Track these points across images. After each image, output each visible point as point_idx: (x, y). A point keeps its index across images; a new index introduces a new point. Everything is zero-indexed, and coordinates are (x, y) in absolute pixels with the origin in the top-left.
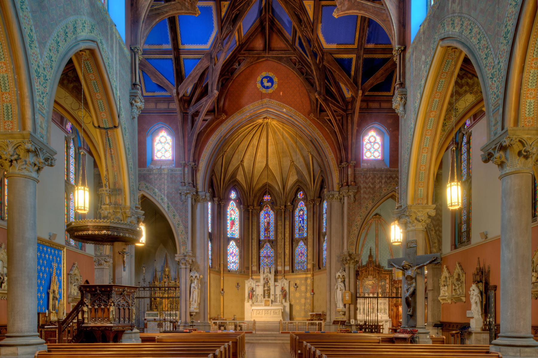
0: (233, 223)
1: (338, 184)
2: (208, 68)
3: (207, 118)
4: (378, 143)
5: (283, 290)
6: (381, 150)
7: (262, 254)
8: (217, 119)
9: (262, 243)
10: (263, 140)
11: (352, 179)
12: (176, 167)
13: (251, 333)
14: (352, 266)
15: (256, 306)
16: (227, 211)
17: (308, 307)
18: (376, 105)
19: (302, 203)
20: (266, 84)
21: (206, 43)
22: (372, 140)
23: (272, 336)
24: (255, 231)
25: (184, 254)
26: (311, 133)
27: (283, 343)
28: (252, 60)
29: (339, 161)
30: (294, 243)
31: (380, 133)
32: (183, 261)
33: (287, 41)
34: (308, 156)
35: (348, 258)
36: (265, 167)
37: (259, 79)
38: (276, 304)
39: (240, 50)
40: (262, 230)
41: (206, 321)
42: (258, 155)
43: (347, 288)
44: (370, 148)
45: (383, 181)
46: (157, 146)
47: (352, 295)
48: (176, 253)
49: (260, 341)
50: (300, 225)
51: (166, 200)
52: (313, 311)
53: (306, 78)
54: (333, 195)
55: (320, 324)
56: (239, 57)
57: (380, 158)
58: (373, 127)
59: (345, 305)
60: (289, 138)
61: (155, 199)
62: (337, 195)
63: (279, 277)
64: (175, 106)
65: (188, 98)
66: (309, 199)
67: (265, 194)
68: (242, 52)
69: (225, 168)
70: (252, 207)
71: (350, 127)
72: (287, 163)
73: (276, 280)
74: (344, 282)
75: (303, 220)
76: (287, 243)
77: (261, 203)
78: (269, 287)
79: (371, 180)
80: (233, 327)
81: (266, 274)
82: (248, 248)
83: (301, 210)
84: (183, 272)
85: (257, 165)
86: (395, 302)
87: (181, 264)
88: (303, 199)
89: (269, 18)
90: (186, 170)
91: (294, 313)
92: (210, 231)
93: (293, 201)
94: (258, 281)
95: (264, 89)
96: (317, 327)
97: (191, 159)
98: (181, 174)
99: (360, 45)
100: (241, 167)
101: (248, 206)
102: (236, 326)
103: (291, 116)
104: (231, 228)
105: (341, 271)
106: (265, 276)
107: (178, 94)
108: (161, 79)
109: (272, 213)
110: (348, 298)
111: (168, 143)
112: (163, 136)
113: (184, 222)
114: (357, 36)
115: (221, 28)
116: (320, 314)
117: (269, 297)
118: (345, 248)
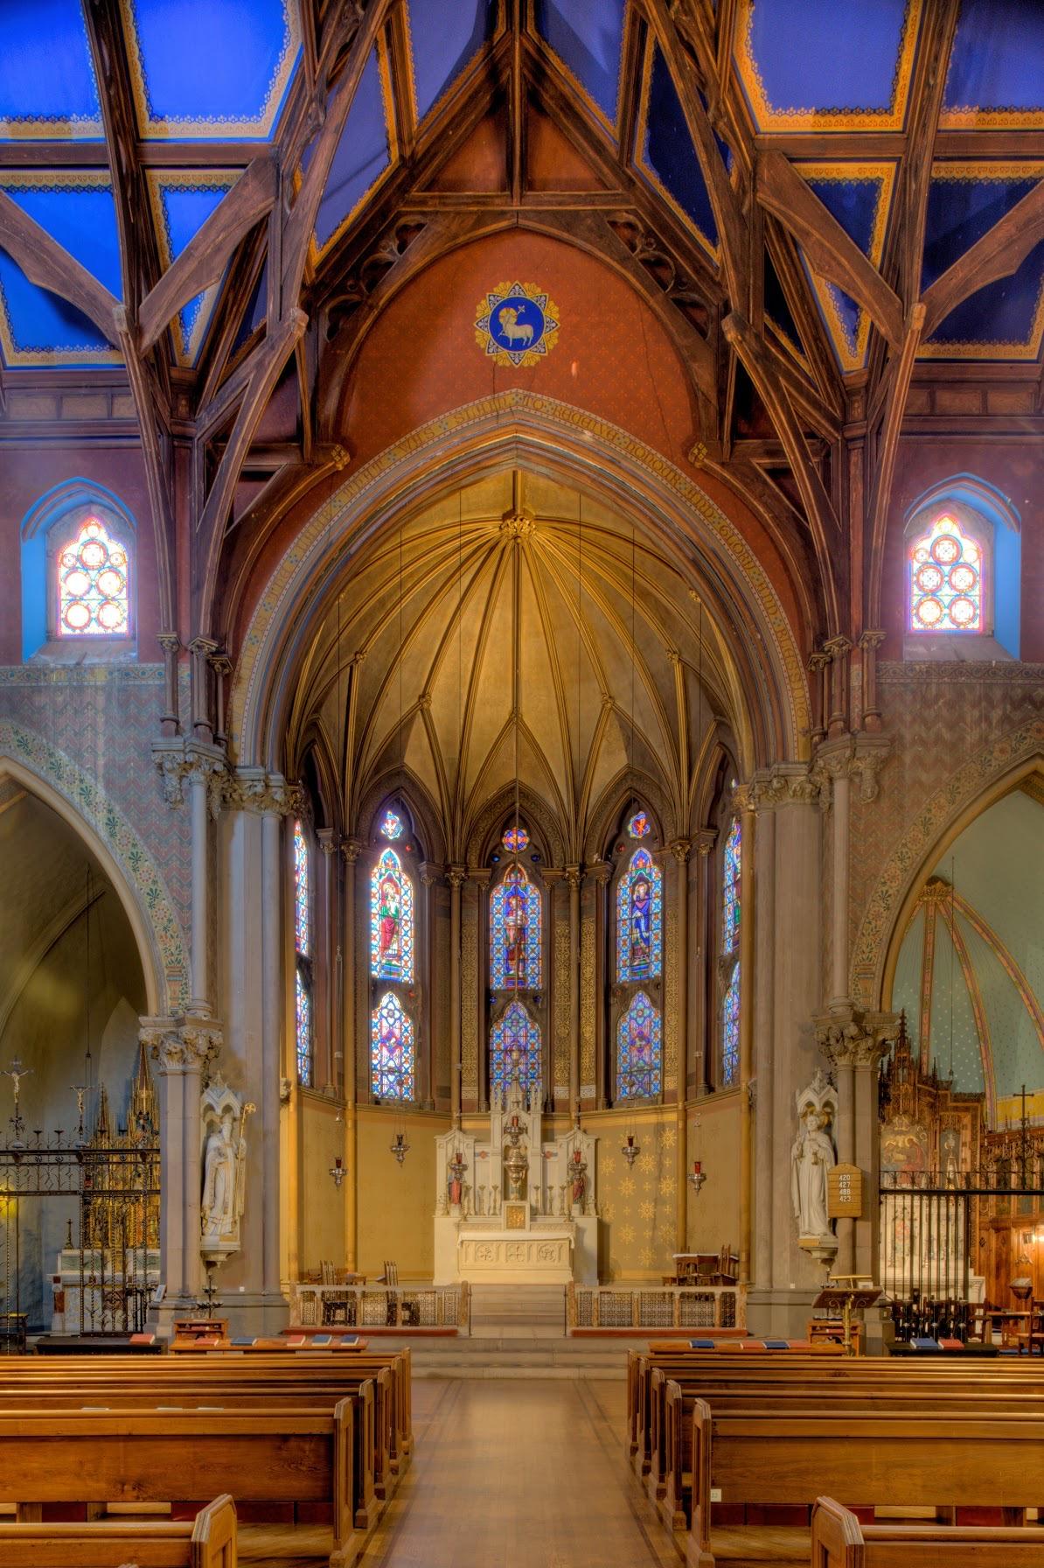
0: (391, 927)
1: (806, 732)
2: (260, 228)
3: (266, 463)
4: (967, 566)
5: (577, 1166)
6: (983, 596)
7: (496, 1043)
8: (311, 466)
9: (498, 1003)
10: (502, 615)
11: (870, 706)
12: (143, 658)
13: (452, 1334)
14: (864, 1063)
15: (476, 1227)
16: (369, 886)
17: (668, 1232)
18: (967, 401)
19: (642, 856)
20: (513, 331)
21: (252, 109)
22: (946, 552)
23: (537, 1347)
24: (472, 958)
25: (174, 1014)
26: (694, 530)
27: (584, 1380)
28: (454, 228)
29: (810, 636)
30: (613, 1000)
31: (981, 525)
32: (171, 1045)
33: (599, 147)
34: (670, 669)
35: (852, 1030)
36: (510, 720)
37: (484, 309)
38: (550, 1220)
39: (404, 189)
40: (498, 954)
41: (271, 1288)
42: (482, 678)
43: (844, 1155)
44: (939, 588)
45: (996, 715)
46: (71, 584)
47: (864, 1180)
48: (145, 1013)
49: (488, 1372)
50: (637, 934)
51: (101, 793)
52: (685, 1249)
53: (676, 301)
54: (785, 778)
55: (729, 1300)
56: (400, 215)
57: (976, 625)
58: (949, 500)
59: (833, 1223)
60: (600, 602)
61: (59, 793)
62: (799, 779)
63: (558, 1125)
64: (132, 407)
65: (190, 377)
66: (669, 835)
67: (507, 826)
68: (415, 193)
69: (358, 719)
70: (459, 870)
71: (856, 496)
72: (589, 704)
73: (547, 1136)
74: (827, 1128)
75: (647, 916)
76: (589, 1002)
77: (492, 856)
78: (523, 1158)
79: (945, 712)
80: (381, 1308)
81: (513, 1101)
82: (449, 1029)
83: (641, 879)
84: (173, 1087)
85: (480, 716)
86: (992, 1214)
87: (165, 1059)
88: (648, 841)
89: (525, 52)
90: (185, 671)
91: (613, 1254)
92: (304, 952)
93: (609, 850)
94: (482, 1137)
95: (504, 352)
96: (717, 1308)
97: (204, 625)
98: (163, 687)
99: (919, 113)
100: (419, 720)
101: (447, 868)
102: (392, 1308)
103: (612, 461)
104: (386, 945)
105: (816, 1084)
106: (507, 1119)
107: (137, 331)
108: (65, 269)
109: (532, 893)
110: (848, 1194)
111: (113, 569)
112: (92, 541)
113: (176, 885)
114: (906, 68)
115: (317, 31)
116: (715, 1259)
117: (523, 1195)
118: (838, 988)
